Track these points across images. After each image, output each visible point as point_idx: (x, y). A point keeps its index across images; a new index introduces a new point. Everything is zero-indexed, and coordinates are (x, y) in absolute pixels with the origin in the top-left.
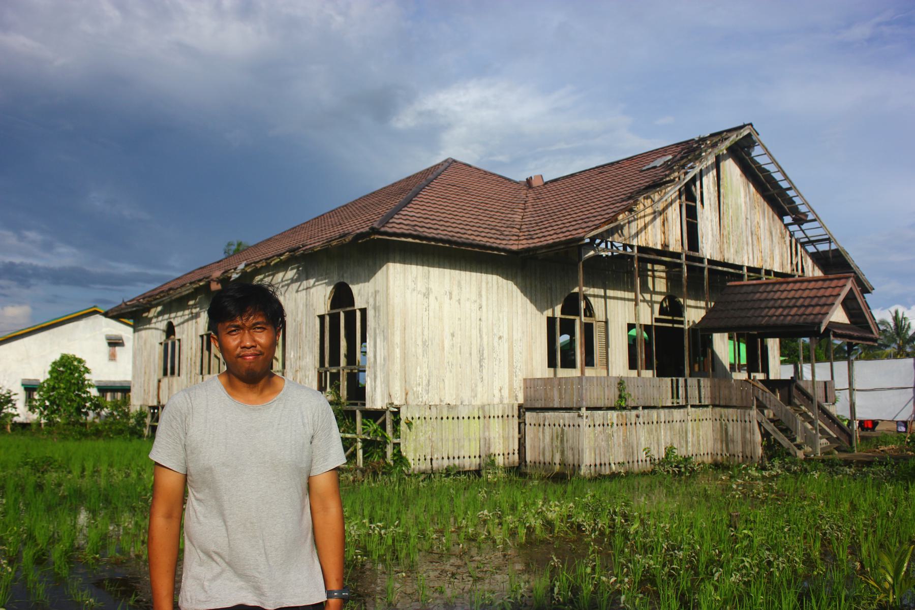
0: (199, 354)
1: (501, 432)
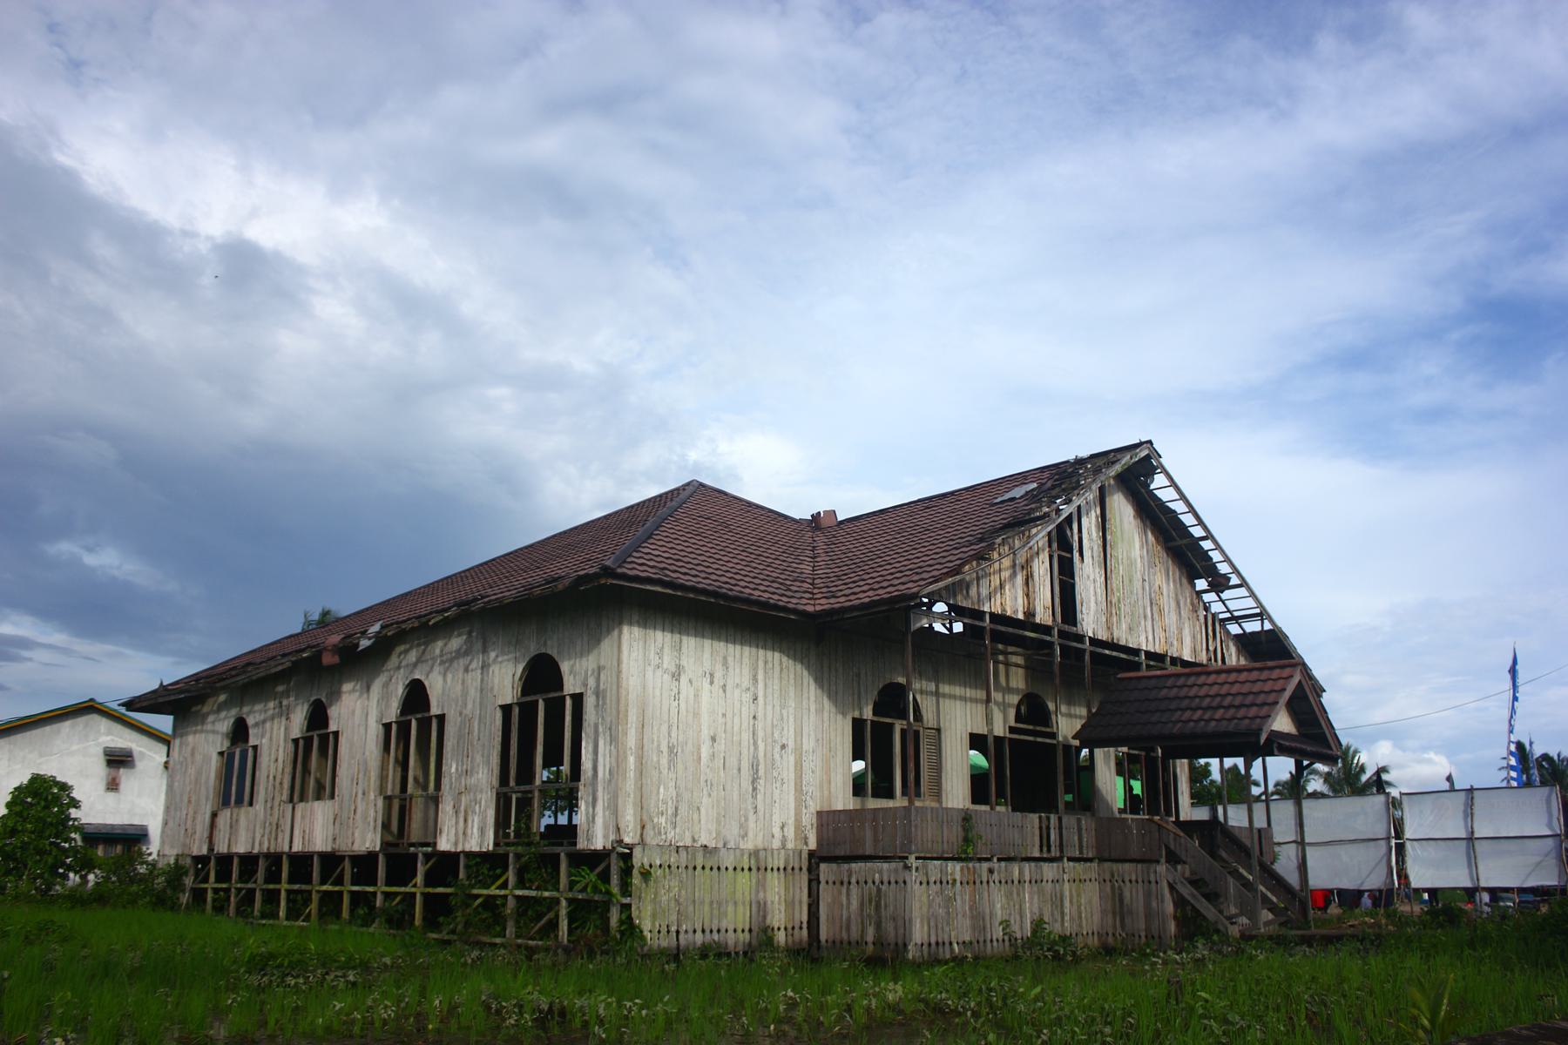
0: (289, 769)
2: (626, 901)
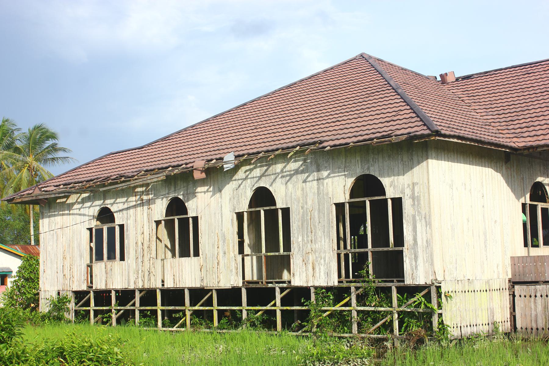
2: (440, 311)
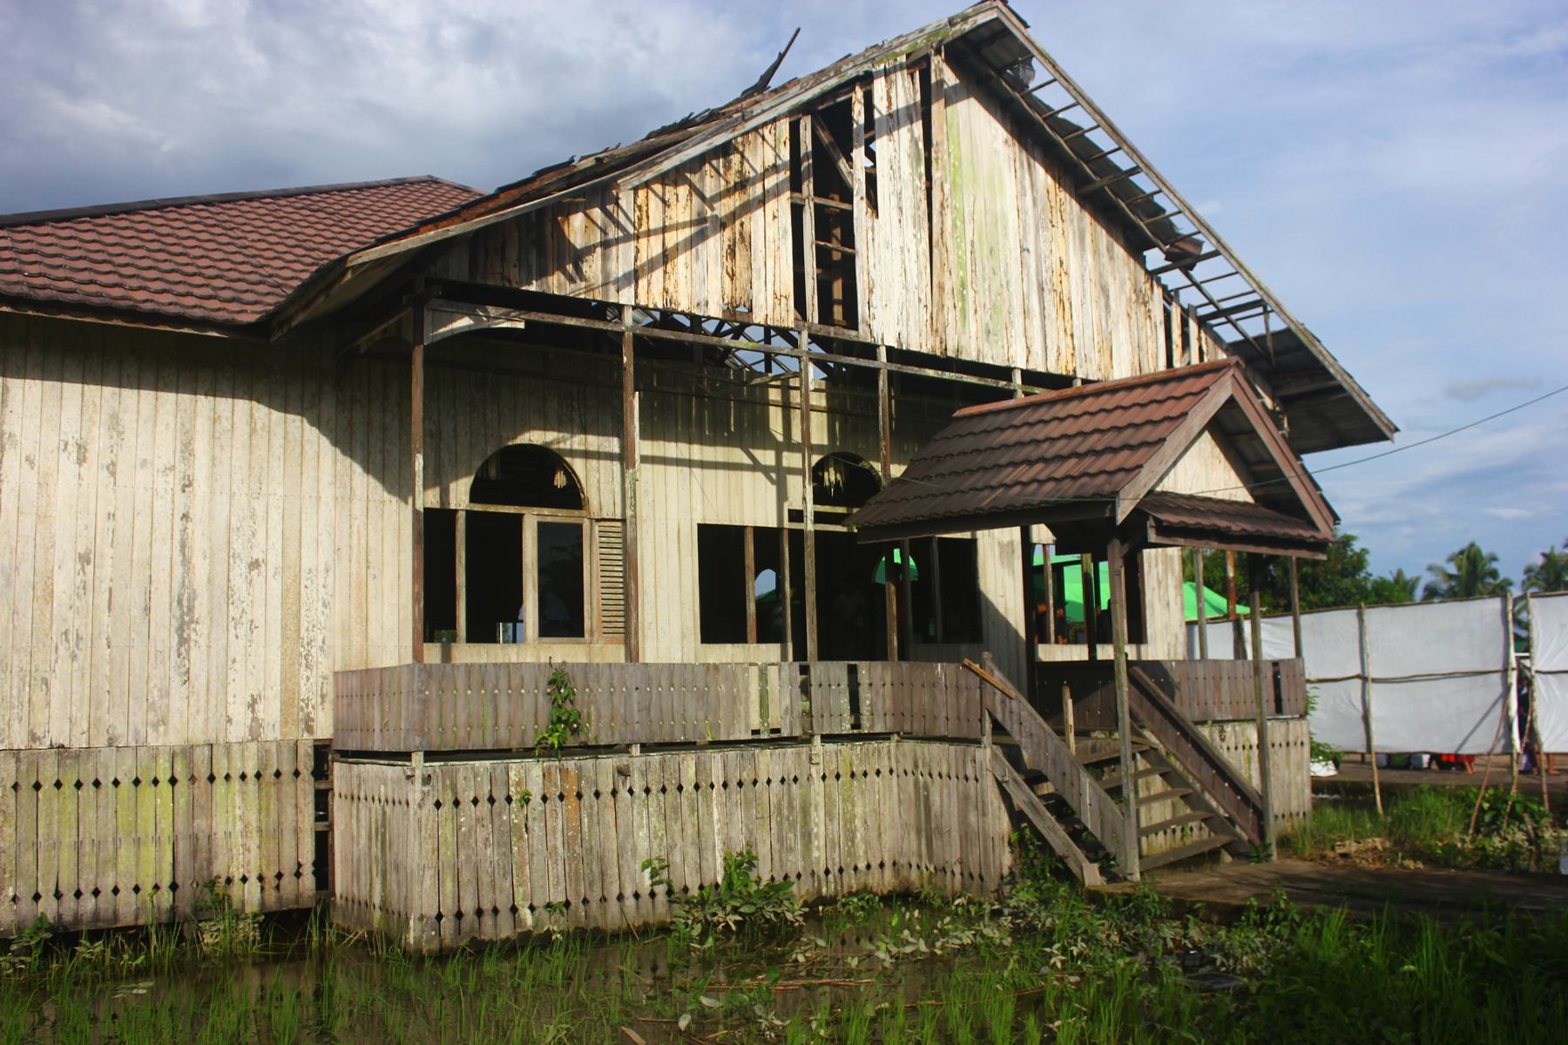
1: (253, 817)
